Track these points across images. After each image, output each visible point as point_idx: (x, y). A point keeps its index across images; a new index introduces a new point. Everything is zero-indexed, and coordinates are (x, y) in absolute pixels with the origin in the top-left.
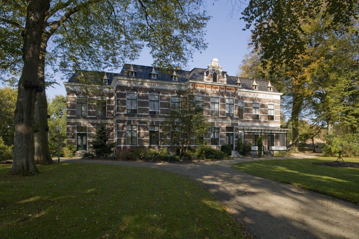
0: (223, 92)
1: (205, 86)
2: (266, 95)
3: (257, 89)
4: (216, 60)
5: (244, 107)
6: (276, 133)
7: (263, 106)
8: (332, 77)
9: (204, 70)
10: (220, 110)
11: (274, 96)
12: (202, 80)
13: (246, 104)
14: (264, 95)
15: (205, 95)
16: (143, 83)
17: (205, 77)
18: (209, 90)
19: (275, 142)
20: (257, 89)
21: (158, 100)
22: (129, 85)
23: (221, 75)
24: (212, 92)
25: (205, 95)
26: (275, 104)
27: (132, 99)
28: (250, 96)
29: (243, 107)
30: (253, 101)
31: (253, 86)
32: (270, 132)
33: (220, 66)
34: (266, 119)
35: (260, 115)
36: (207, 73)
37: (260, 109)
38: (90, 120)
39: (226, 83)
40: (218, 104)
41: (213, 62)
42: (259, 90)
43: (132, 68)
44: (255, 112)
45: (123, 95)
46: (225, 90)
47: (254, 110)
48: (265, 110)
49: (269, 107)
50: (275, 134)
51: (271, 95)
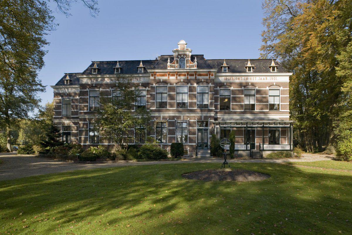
0: (191, 79)
1: (169, 75)
2: (265, 77)
3: (252, 71)
4: (183, 42)
5: (231, 96)
6: (282, 127)
7: (258, 92)
8: (338, 38)
9: (168, 56)
10: (189, 101)
11: (278, 78)
12: (166, 68)
13: (233, 92)
14: (263, 78)
15: (169, 85)
16: (103, 79)
17: (169, 64)
18: (172, 79)
19: (256, 139)
20: (252, 71)
21: (279, 95)
22: (89, 82)
23: (190, 59)
24: (177, 81)
25: (169, 85)
26: (281, 88)
27: (94, 97)
28: (237, 81)
29: (230, 96)
30: (245, 87)
31: (246, 67)
32: (262, 126)
33: (189, 49)
34: (262, 109)
35: (256, 103)
36: (172, 59)
37: (256, 96)
38: (72, 120)
39: (195, 68)
40: (207, 94)
41: (179, 46)
42: (254, 72)
43: (141, 63)
44: (247, 101)
45: (86, 93)
46: (210, 76)
47: (245, 98)
48: (262, 97)
49: (271, 93)
50: (280, 129)
51: (273, 77)
